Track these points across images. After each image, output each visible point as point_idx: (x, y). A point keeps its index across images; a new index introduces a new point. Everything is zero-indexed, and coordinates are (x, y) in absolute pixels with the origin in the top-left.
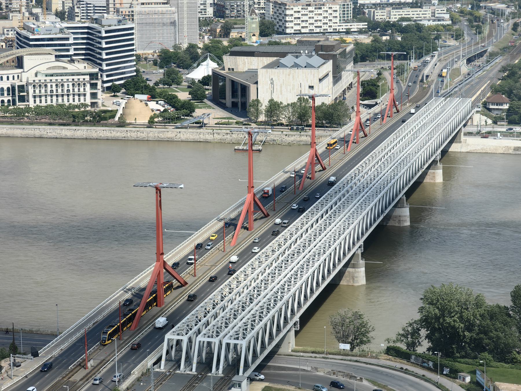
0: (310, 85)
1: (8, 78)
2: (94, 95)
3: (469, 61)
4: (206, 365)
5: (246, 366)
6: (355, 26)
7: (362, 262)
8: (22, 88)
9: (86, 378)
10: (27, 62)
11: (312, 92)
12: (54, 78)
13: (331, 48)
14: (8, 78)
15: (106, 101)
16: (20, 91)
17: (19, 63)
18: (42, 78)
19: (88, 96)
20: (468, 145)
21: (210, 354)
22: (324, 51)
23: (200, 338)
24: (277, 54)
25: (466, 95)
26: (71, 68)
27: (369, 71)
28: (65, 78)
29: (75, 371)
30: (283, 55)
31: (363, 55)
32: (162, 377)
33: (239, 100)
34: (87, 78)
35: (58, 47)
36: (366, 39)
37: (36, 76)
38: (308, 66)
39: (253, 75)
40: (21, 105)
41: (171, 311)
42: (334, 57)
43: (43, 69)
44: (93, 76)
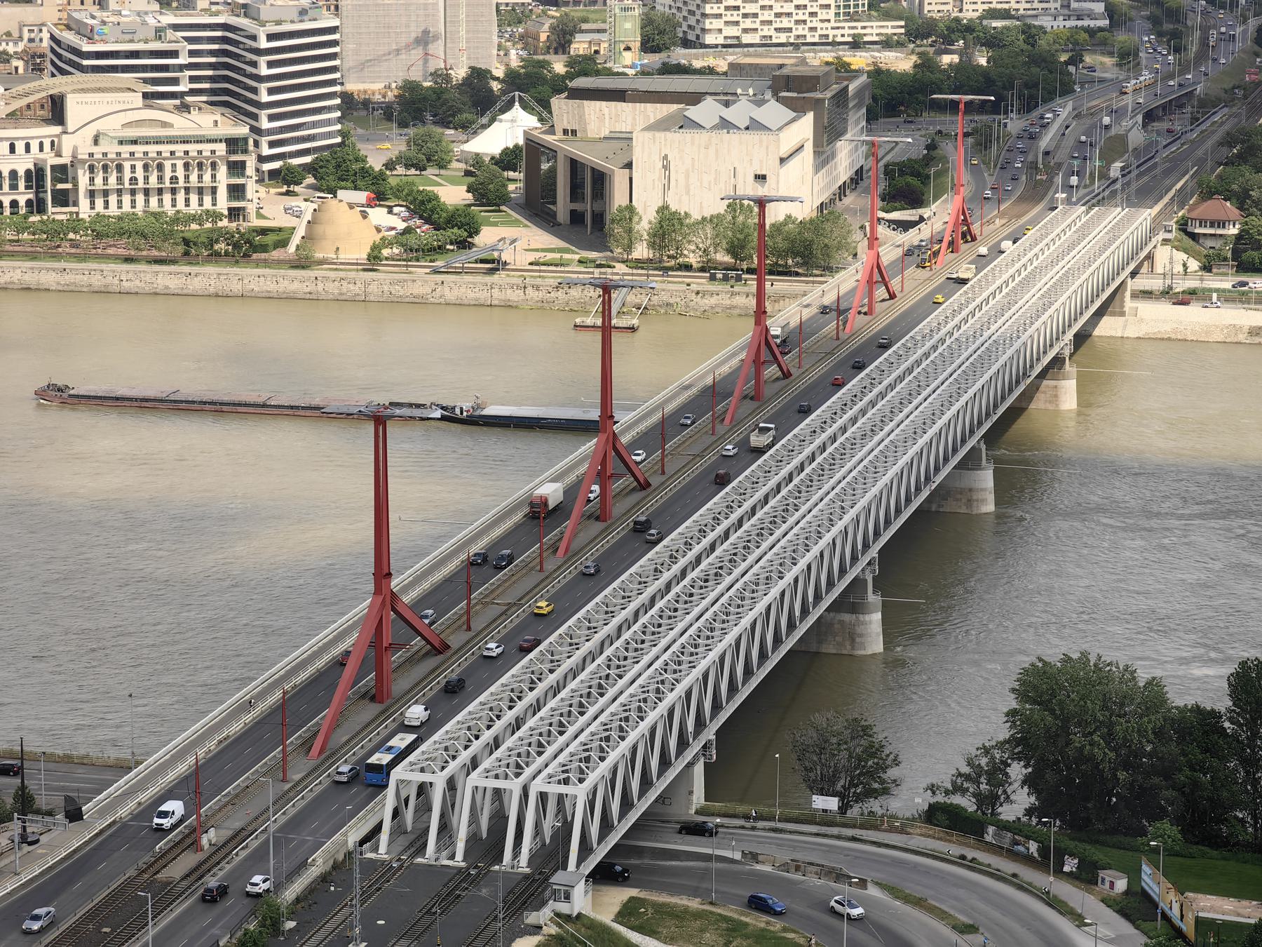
1: (28, 148)
2: (236, 191)
3: (1150, 117)
4: (487, 847)
7: (873, 598)
8: (62, 172)
9: (197, 872)
10: (75, 109)
11: (761, 191)
12: (139, 149)
14: (28, 148)
15: (268, 207)
16: (56, 180)
17: (56, 111)
18: (112, 149)
19: (222, 193)
20: (1145, 319)
21: (499, 818)
22: (792, 88)
23: (475, 778)
26: (181, 124)
27: (904, 142)
28: (166, 149)
33: (587, 207)
34: (221, 148)
35: (155, 74)
36: (901, 62)
37: (96, 142)
40: (58, 214)
43: (112, 125)
44: (234, 144)
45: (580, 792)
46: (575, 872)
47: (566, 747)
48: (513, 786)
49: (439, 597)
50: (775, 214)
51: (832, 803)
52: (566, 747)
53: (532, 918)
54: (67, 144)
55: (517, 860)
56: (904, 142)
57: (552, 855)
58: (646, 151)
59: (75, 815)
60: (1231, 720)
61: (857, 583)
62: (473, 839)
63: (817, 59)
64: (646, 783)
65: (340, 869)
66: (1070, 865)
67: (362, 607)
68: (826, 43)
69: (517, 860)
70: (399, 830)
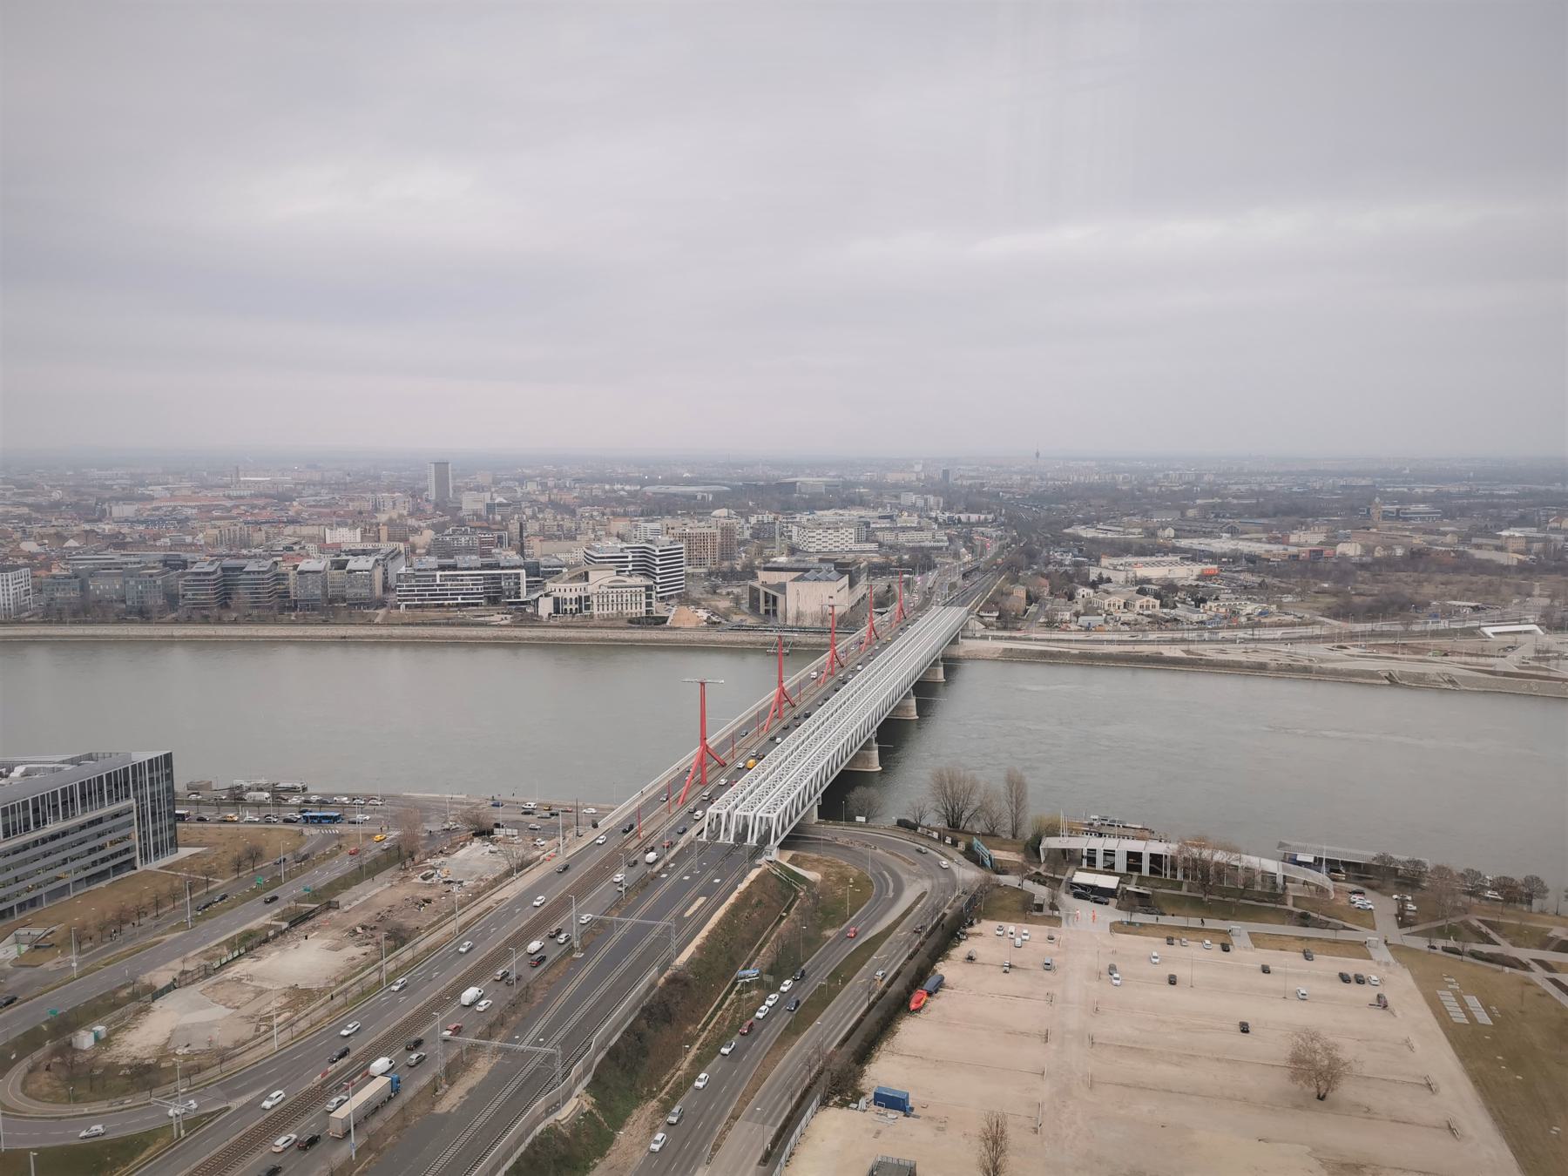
0: (943, 993)
2: (649, 605)
3: (965, 576)
4: (742, 836)
5: (776, 838)
6: (868, 546)
7: (876, 745)
8: (587, 598)
11: (832, 602)
13: (848, 565)
15: (658, 609)
17: (586, 577)
18: (605, 590)
20: (968, 646)
21: (746, 827)
22: (842, 568)
24: (803, 573)
25: (963, 604)
26: (630, 581)
27: (880, 584)
29: (251, 1044)
30: (806, 570)
31: (876, 570)
32: (704, 846)
33: (771, 608)
35: (619, 563)
36: (877, 559)
38: (828, 580)
39: (782, 588)
41: (106, 1103)
42: (850, 572)
43: (606, 582)
44: (648, 588)
45: (775, 816)
46: (773, 844)
47: (768, 800)
48: (751, 814)
49: (723, 746)
50: (838, 610)
51: (863, 819)
52: (768, 800)
53: (758, 862)
54: (590, 589)
55: (752, 841)
56: (880, 584)
57: (764, 839)
58: (791, 588)
59: (595, 826)
60: (587, 1135)
61: (869, 740)
62: (737, 834)
63: (850, 557)
64: (797, 813)
65: (692, 843)
66: (948, 841)
67: (697, 749)
68: (851, 551)
69: (752, 841)
70: (710, 831)
